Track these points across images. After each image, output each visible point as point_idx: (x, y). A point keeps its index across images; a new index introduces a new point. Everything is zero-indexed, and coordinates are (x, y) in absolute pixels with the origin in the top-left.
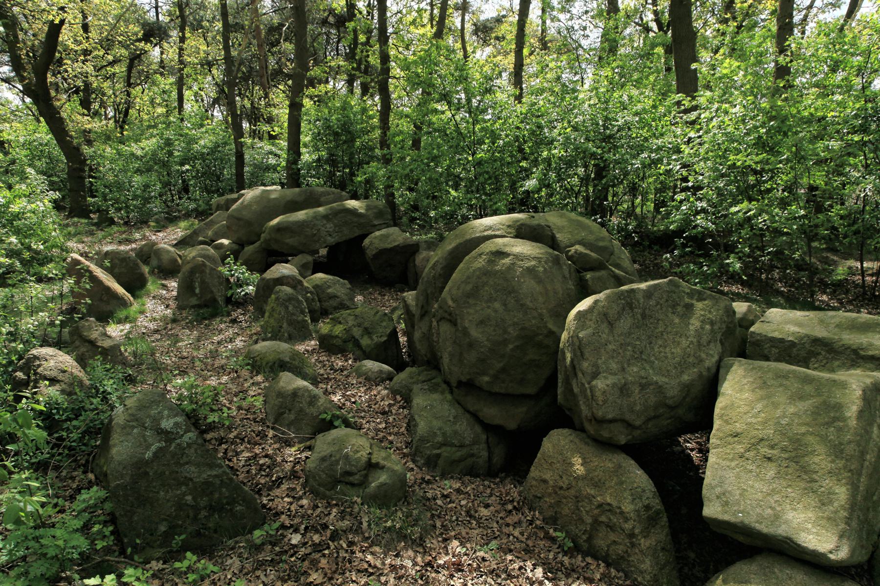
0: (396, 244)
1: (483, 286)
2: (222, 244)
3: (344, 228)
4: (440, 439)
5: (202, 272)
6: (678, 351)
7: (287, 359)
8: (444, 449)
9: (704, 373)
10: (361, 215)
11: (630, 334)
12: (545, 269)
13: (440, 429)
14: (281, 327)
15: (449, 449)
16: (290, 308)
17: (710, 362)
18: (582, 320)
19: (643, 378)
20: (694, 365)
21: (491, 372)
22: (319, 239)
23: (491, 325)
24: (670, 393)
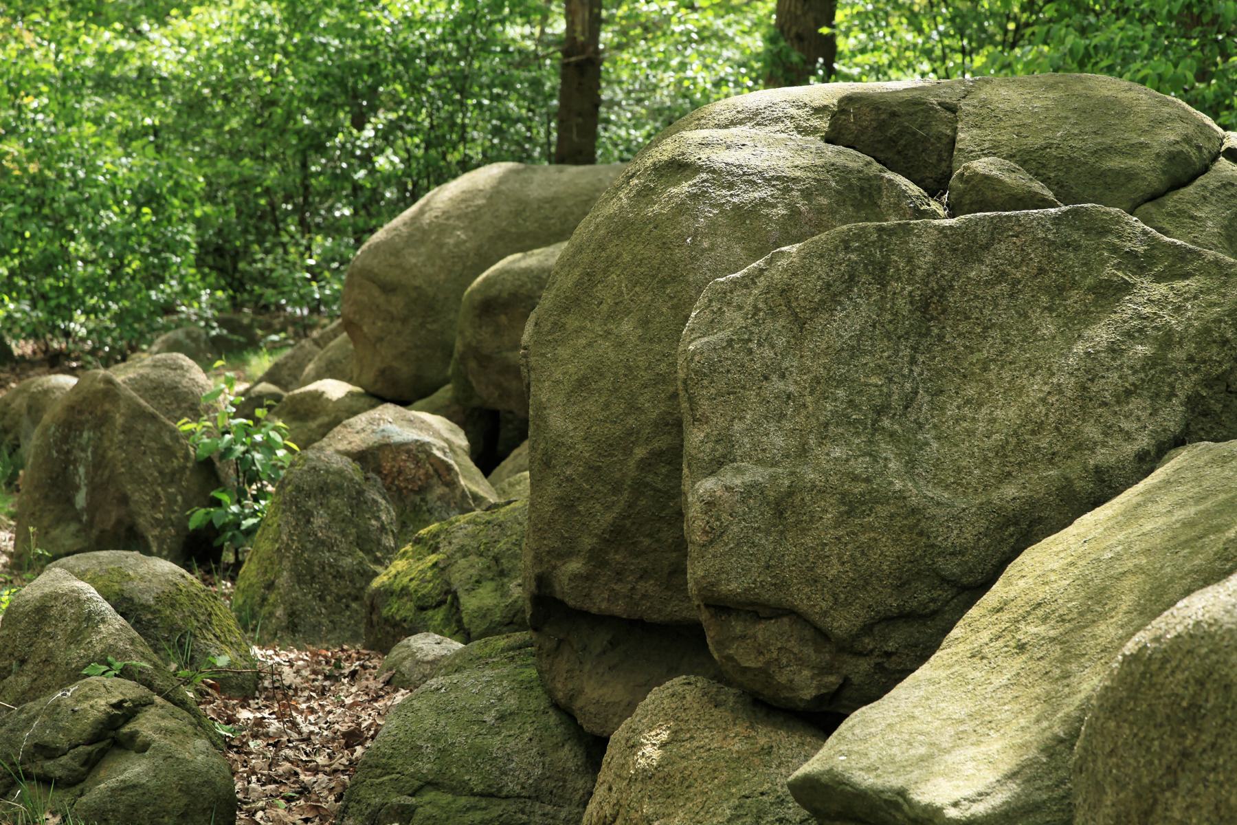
1: (605, 271)
2: (318, 396)
4: (426, 767)
5: (103, 421)
6: (1009, 414)
8: (430, 796)
9: (1078, 485)
11: (855, 351)
13: (435, 738)
14: (270, 586)
15: (445, 798)
16: (317, 522)
18: (715, 306)
19: (855, 478)
20: (1051, 459)
21: (587, 542)
23: (599, 391)
24: (951, 537)
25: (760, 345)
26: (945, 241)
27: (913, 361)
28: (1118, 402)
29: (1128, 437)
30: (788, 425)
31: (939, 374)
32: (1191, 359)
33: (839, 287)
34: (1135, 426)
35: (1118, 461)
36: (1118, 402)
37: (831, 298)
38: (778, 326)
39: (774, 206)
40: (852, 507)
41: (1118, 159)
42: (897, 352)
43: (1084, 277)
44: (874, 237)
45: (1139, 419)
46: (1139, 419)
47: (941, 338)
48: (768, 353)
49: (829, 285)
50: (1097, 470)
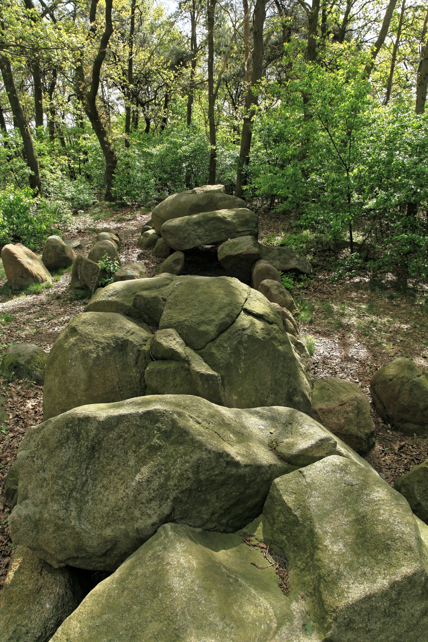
0: (239, 252)
3: (214, 233)
7: (23, 362)
9: (131, 534)
10: (228, 223)
12: (98, 356)
17: (143, 523)
19: (60, 518)
22: (189, 242)
25: (37, 459)
27: (87, 468)
28: (147, 503)
29: (150, 516)
30: (44, 490)
31: (96, 472)
32: (175, 485)
34: (153, 512)
37: (61, 444)
38: (45, 451)
39: (93, 353)
40: (58, 528)
41: (205, 326)
42: (80, 467)
43: (147, 441)
44: (77, 422)
45: (154, 509)
46: (154, 509)
47: (99, 458)
48: (40, 462)
49: (60, 440)
50: (137, 529)
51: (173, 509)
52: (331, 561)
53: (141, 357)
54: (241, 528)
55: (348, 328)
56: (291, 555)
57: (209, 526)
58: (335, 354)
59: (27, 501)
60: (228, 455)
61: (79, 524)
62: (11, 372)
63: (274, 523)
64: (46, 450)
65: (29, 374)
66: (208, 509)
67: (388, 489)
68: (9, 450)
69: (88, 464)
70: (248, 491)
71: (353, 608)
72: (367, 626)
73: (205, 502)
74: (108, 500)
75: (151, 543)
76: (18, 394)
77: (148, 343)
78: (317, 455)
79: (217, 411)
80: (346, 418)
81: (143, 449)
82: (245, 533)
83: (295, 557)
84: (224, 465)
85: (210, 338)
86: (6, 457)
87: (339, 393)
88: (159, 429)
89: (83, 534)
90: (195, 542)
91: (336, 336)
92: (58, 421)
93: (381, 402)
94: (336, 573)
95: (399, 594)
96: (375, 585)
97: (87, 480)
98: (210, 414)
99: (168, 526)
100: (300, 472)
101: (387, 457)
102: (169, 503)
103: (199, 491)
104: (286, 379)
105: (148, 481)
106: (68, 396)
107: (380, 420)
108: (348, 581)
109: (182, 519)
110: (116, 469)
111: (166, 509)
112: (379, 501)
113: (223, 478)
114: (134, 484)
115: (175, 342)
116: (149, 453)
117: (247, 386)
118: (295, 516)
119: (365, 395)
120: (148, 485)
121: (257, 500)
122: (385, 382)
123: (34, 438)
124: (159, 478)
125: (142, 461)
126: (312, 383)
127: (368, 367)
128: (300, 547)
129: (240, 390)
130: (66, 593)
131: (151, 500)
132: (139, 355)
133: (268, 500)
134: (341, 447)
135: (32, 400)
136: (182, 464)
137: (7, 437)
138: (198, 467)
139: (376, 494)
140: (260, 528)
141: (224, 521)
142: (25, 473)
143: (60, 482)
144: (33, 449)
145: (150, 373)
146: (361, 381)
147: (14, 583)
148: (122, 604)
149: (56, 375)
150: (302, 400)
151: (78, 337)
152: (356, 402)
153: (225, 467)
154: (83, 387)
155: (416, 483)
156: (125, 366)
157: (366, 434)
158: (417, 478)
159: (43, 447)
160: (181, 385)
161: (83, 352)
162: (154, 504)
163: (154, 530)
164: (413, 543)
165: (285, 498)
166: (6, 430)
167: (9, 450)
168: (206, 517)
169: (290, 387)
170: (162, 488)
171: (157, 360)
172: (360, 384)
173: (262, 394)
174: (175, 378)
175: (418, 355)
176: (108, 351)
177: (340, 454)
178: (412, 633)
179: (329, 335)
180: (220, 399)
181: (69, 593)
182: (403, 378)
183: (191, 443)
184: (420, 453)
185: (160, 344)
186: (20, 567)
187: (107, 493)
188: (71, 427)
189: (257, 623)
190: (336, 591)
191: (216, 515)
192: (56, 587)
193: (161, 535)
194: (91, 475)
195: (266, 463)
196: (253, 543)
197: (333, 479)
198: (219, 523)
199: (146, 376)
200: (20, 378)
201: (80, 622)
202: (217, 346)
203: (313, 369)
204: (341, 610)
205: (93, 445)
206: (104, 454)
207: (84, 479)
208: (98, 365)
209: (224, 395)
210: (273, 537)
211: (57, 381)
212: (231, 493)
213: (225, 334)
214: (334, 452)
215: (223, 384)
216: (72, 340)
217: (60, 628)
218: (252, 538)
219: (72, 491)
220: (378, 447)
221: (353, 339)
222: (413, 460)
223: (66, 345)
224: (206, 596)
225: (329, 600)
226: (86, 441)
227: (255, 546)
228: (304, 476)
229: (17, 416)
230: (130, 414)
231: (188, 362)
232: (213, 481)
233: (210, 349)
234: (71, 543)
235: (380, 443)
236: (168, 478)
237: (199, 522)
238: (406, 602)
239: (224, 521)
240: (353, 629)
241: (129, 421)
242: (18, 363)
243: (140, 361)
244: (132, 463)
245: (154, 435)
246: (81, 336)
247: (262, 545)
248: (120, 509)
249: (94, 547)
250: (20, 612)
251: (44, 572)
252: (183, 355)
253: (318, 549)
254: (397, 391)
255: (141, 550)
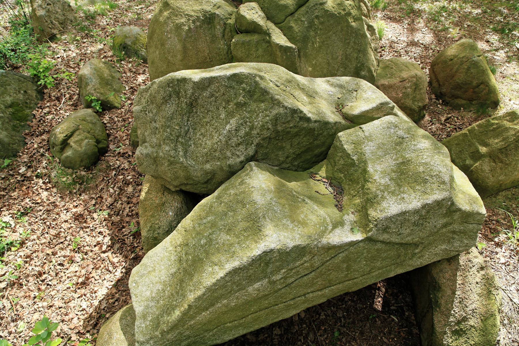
7: (129, 43)
9: (225, 168)
12: (190, 28)
19: (171, 156)
25: (149, 112)
26: (195, 86)
27: (188, 120)
28: (236, 146)
29: (238, 156)
32: (258, 134)
33: (167, 98)
34: (241, 153)
35: (235, 163)
36: (236, 146)
37: (165, 101)
39: (185, 25)
43: (234, 99)
44: (176, 83)
47: (196, 112)
48: (151, 115)
49: (164, 98)
51: (256, 152)
52: (378, 190)
53: (228, 30)
54: (308, 169)
55: (418, 13)
56: (347, 187)
57: (284, 166)
58: (402, 39)
59: (146, 144)
60: (301, 112)
61: (186, 160)
62: (121, 52)
63: (335, 165)
64: (155, 105)
65: (136, 53)
66: (284, 154)
67: (434, 141)
68: (129, 114)
69: (189, 117)
70: (315, 142)
71: (391, 219)
72: (399, 231)
73: (282, 148)
74: (206, 144)
75: (240, 174)
76: (130, 70)
77: (233, 17)
78: (376, 116)
79: (293, 77)
80: (404, 93)
81: (231, 106)
82: (312, 172)
83: (349, 189)
84: (298, 120)
85: (289, 11)
86: (128, 118)
87: (401, 71)
88: (244, 90)
89: (190, 168)
90: (274, 175)
91: (406, 22)
92: (161, 82)
93: (438, 81)
94: (381, 197)
95: (428, 212)
96: (410, 205)
97: (189, 130)
98: (287, 79)
99: (252, 163)
100: (361, 128)
101: (433, 126)
102: (253, 147)
103: (277, 140)
104: (355, 55)
105: (236, 130)
106: (168, 65)
107: (433, 96)
108: (389, 202)
109: (263, 159)
110: (211, 121)
111: (251, 151)
112: (424, 149)
113: (296, 130)
114: (225, 132)
115: (257, 15)
116: (236, 108)
117: (320, 60)
118: (353, 160)
119: (425, 74)
120: (236, 133)
121: (323, 149)
122: (445, 62)
123: (144, 96)
124: (245, 128)
125: (230, 115)
126: (379, 62)
127: (431, 51)
128: (353, 181)
129: (314, 62)
130: (182, 207)
131: (239, 144)
132: (225, 28)
133: (331, 149)
134: (397, 110)
135: (142, 76)
136: (262, 117)
137: (126, 104)
138: (276, 120)
139: (423, 145)
140: (324, 169)
141: (296, 163)
142: (141, 123)
143: (168, 130)
144: (144, 104)
145: (236, 44)
146: (422, 63)
147: (145, 199)
148: (221, 211)
149: (156, 47)
150: (367, 74)
151: (171, 10)
152: (415, 79)
153: (299, 122)
154: (179, 57)
155: (455, 146)
156: (214, 39)
157: (420, 107)
158: (456, 142)
159: (152, 103)
160: (263, 56)
161: (177, 25)
162: (241, 147)
163: (242, 165)
164: (447, 179)
165: (345, 146)
166: (125, 98)
167: (129, 114)
168: (281, 159)
169: (358, 63)
170: (247, 135)
171: (241, 33)
172: (421, 65)
173: (333, 67)
174: (257, 50)
175: (482, 39)
176: (198, 24)
177: (395, 115)
178: (432, 238)
179: (399, 21)
180: (296, 69)
181: (184, 207)
182: (463, 57)
183: (271, 101)
184: (463, 124)
185: (243, 17)
186: (149, 190)
187: (205, 139)
188: (172, 87)
189: (318, 226)
190: (379, 208)
191: (290, 159)
192: (175, 203)
193: (248, 170)
194: (191, 126)
195: (332, 120)
196: (317, 179)
197: (388, 134)
198: (292, 165)
199: (232, 48)
200: (130, 58)
201: (192, 221)
202: (296, 20)
203: (380, 52)
204: (381, 220)
205: (192, 102)
206: (200, 109)
207: (186, 128)
208: (191, 37)
209: (300, 65)
210: (333, 175)
211: (157, 52)
212: (302, 142)
213: (303, 9)
214: (390, 112)
215: (299, 56)
216: (166, 14)
217: (180, 225)
218: (317, 176)
219: (178, 137)
220: (427, 118)
221: (422, 25)
222: (456, 129)
223: (161, 19)
224: (281, 208)
225: (373, 213)
226: (185, 98)
227: (319, 180)
228: (363, 131)
229: (132, 88)
230: (220, 76)
231: (269, 35)
232: (288, 132)
233: (289, 23)
234: (182, 174)
235: (429, 115)
236: (252, 128)
237: (276, 163)
238: (432, 218)
239: (296, 163)
240: (388, 233)
241: (219, 83)
242: (125, 44)
243: (226, 34)
244: (223, 116)
245: (240, 94)
246: (173, 9)
247: (324, 180)
248: (215, 151)
249: (198, 177)
250: (153, 216)
251: (166, 194)
252: (265, 28)
253: (368, 181)
254: (454, 70)
255: (233, 179)
